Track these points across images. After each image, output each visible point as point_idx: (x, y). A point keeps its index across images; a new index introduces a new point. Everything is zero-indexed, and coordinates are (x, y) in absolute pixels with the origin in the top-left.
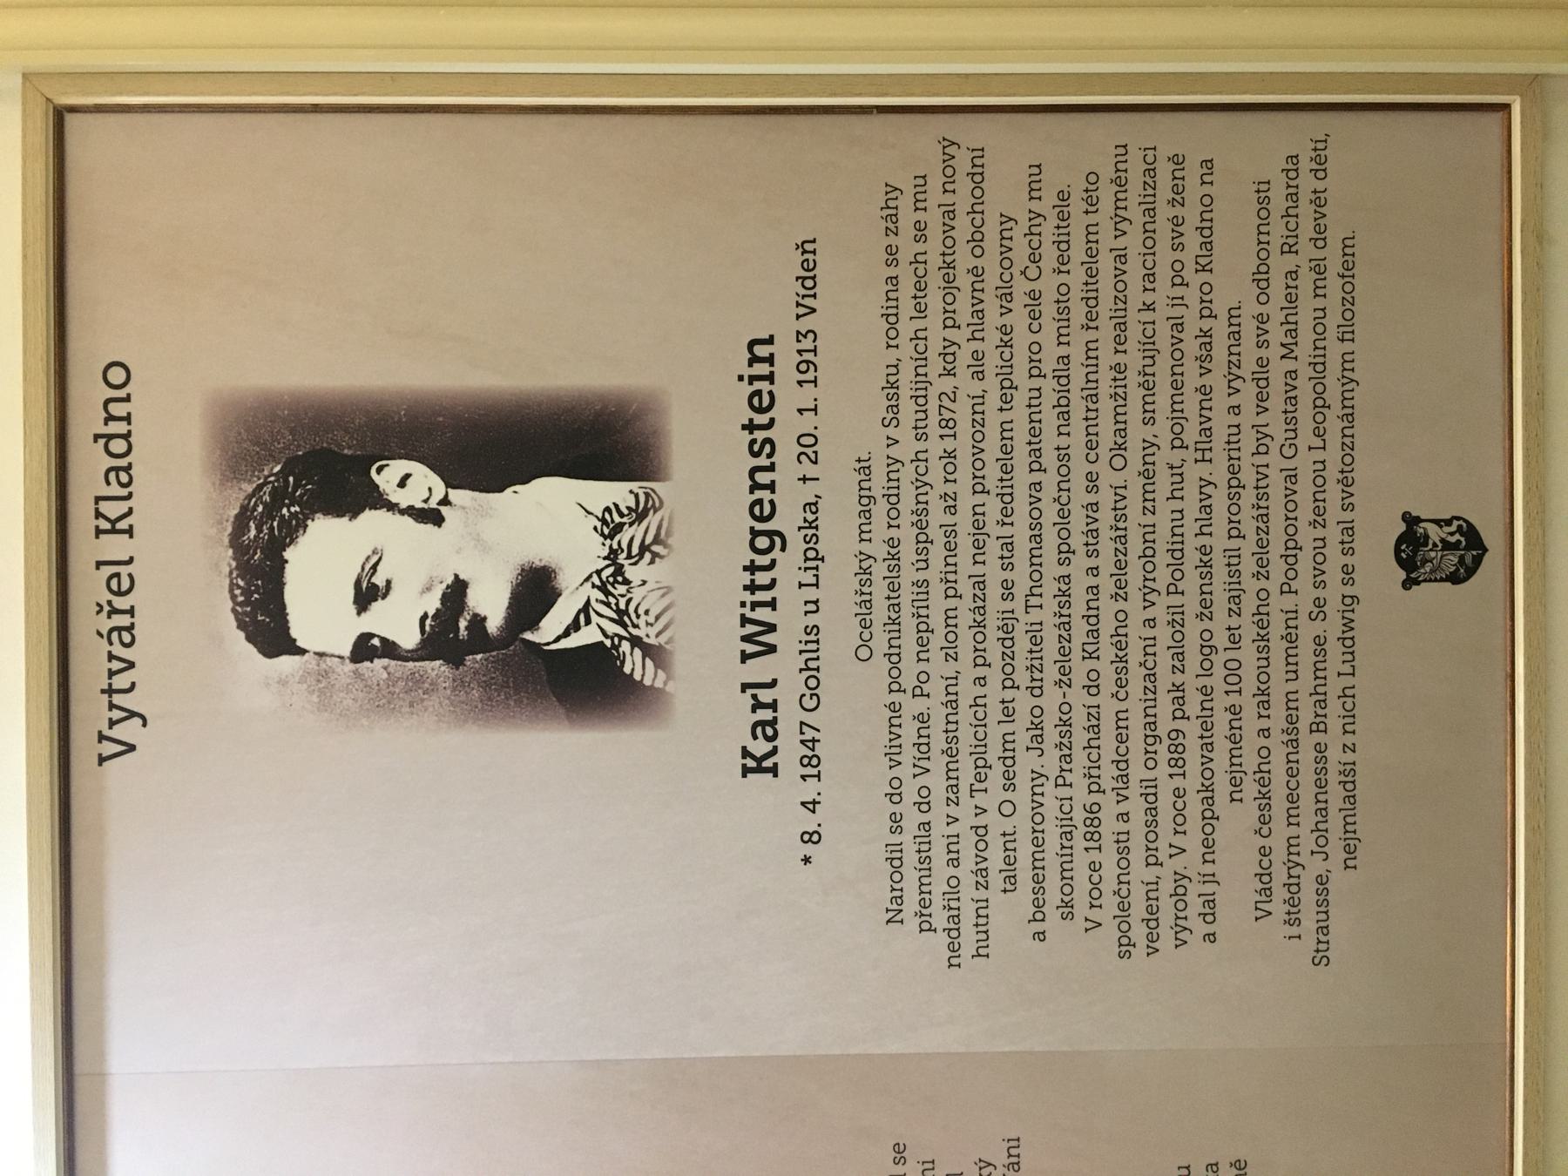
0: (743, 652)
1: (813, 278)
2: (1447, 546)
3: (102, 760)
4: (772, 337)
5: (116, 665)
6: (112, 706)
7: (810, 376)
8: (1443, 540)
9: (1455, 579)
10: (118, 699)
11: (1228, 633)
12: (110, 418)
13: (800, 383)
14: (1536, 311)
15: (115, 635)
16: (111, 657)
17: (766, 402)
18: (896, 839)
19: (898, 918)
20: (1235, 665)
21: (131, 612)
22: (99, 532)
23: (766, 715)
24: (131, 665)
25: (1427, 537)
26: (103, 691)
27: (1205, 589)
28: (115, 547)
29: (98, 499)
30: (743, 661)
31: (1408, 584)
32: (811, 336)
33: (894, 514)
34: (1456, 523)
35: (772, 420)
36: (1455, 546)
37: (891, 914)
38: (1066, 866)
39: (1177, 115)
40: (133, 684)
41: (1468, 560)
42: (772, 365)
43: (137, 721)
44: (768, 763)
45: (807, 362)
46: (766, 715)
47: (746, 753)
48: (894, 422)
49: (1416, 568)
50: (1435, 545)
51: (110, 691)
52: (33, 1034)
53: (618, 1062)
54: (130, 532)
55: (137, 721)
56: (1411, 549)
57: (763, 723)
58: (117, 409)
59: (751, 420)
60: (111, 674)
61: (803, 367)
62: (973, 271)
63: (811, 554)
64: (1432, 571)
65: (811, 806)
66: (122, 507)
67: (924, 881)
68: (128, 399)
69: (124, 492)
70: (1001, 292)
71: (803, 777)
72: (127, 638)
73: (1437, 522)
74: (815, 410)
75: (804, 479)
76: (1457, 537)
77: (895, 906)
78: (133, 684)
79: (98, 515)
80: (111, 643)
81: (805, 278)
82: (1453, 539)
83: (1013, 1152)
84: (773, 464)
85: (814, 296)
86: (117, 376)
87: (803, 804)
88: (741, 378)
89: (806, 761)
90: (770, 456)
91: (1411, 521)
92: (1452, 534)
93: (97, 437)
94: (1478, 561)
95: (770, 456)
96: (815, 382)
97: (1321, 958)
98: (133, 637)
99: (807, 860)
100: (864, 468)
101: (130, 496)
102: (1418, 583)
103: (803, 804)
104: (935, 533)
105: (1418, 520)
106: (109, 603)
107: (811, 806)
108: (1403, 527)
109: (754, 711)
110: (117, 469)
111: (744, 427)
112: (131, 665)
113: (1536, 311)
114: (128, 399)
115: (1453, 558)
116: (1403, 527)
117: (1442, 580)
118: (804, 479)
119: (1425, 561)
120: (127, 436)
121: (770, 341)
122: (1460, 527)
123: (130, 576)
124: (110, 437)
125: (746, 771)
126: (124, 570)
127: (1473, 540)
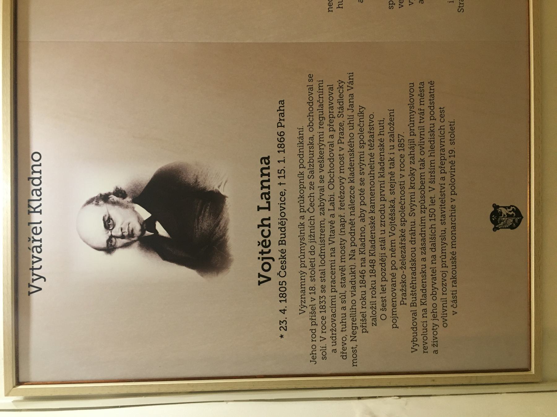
0: (259, 281)
1: (285, 228)
2: (509, 216)
3: (30, 293)
4: (270, 218)
8: (507, 214)
9: (512, 227)
10: (35, 272)
11: (430, 199)
15: (35, 249)
16: (33, 257)
17: (268, 244)
18: (311, 83)
20: (433, 211)
21: (40, 241)
23: (266, 190)
24: (40, 259)
25: (501, 213)
26: (30, 269)
27: (424, 281)
30: (259, 285)
31: (495, 229)
33: (314, 336)
34: (512, 208)
35: (270, 251)
36: (512, 216)
40: (41, 266)
42: (269, 176)
43: (42, 279)
46: (266, 190)
48: (312, 177)
49: (498, 224)
50: (504, 215)
51: (33, 269)
52: (3, 23)
53: (210, 43)
54: (40, 212)
55: (42, 279)
56: (496, 217)
59: (262, 250)
60: (33, 263)
63: (283, 230)
64: (504, 225)
65: (283, 311)
67: (322, 248)
68: (40, 165)
70: (350, 206)
71: (279, 152)
72: (39, 250)
73: (505, 207)
74: (284, 161)
75: (280, 184)
76: (512, 212)
78: (41, 266)
80: (33, 252)
81: (281, 228)
83: (351, 78)
84: (269, 167)
85: (285, 204)
87: (280, 311)
88: (259, 258)
89: (279, 146)
91: (496, 207)
92: (510, 212)
94: (520, 221)
97: (461, 9)
98: (41, 193)
99: (282, 336)
101: (41, 199)
102: (499, 229)
103: (280, 311)
104: (328, 309)
105: (498, 207)
106: (33, 237)
107: (283, 311)
109: (262, 189)
110: (36, 190)
111: (260, 253)
112: (40, 259)
114: (40, 165)
116: (493, 209)
117: (507, 228)
119: (501, 221)
120: (40, 178)
121: (269, 219)
122: (513, 209)
123: (40, 228)
126: (38, 226)
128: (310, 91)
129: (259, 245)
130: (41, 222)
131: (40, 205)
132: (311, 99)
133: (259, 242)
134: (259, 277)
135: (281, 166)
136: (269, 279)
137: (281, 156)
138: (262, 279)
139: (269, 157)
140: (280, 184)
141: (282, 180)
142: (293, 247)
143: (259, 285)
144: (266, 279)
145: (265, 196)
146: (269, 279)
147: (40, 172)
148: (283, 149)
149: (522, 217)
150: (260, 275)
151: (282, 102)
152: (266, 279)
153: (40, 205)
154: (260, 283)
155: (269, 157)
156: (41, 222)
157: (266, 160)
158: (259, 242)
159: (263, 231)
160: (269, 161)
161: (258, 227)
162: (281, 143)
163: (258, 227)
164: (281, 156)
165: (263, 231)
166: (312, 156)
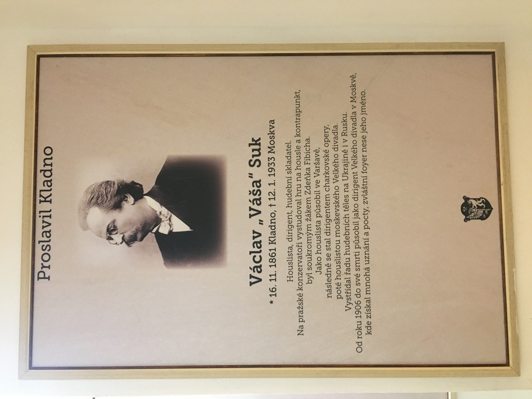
0: (250, 282)
2: (479, 207)
5: (45, 224)
6: (43, 222)
7: (273, 173)
8: (477, 205)
9: (482, 218)
12: (46, 165)
13: (269, 175)
14: (513, 319)
19: (302, 333)
22: (41, 201)
24: (50, 224)
25: (472, 204)
28: (45, 206)
29: (41, 191)
30: (250, 217)
31: (466, 220)
32: (273, 159)
37: (299, 332)
38: (357, 262)
39: (398, 364)
41: (486, 212)
44: (258, 142)
45: (272, 168)
47: (270, 240)
49: (469, 215)
50: (475, 207)
56: (466, 208)
57: (257, 242)
58: (48, 162)
61: (270, 170)
62: (328, 265)
64: (474, 216)
66: (48, 193)
69: (49, 188)
74: (274, 184)
76: (482, 204)
77: (300, 329)
79: (41, 196)
82: (481, 205)
86: (48, 151)
89: (271, 260)
90: (259, 195)
91: (466, 199)
92: (480, 203)
93: (41, 171)
94: (490, 212)
95: (259, 195)
96: (274, 175)
99: (271, 302)
100: (289, 146)
101: (51, 190)
102: (469, 220)
105: (468, 199)
106: (42, 264)
108: (463, 201)
110: (47, 181)
113: (513, 319)
114: (51, 158)
115: (481, 212)
116: (463, 201)
117: (477, 219)
118: (271, 205)
122: (483, 201)
124: (45, 171)
125: (270, 243)
127: (487, 205)
128: (299, 260)
129: (250, 194)
130: (50, 211)
131: (51, 195)
132: (299, 212)
133: (250, 191)
134: (250, 278)
135: (271, 189)
136: (260, 280)
137: (271, 179)
138: (253, 280)
139: (260, 180)
140: (271, 205)
141: (272, 202)
142: (282, 246)
143: (250, 217)
144: (257, 280)
145: (256, 202)
146: (260, 280)
147: (51, 165)
148: (274, 264)
149: (492, 209)
150: (251, 209)
151: (272, 121)
152: (257, 280)
153: (51, 195)
154: (251, 284)
155: (260, 180)
156: (50, 211)
157: (256, 142)
158: (250, 191)
159: (255, 256)
160: (261, 245)
161: (250, 254)
162: (272, 258)
163: (250, 254)
164: (271, 179)
165: (255, 256)
166: (298, 106)
